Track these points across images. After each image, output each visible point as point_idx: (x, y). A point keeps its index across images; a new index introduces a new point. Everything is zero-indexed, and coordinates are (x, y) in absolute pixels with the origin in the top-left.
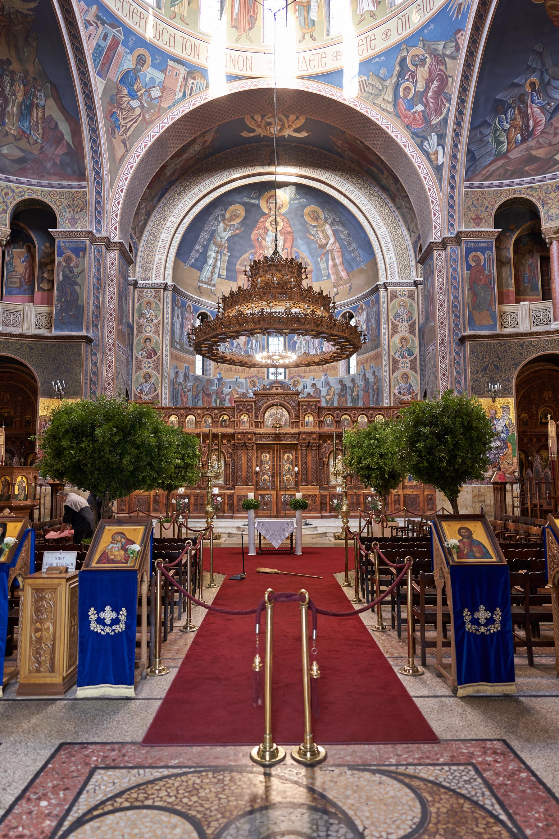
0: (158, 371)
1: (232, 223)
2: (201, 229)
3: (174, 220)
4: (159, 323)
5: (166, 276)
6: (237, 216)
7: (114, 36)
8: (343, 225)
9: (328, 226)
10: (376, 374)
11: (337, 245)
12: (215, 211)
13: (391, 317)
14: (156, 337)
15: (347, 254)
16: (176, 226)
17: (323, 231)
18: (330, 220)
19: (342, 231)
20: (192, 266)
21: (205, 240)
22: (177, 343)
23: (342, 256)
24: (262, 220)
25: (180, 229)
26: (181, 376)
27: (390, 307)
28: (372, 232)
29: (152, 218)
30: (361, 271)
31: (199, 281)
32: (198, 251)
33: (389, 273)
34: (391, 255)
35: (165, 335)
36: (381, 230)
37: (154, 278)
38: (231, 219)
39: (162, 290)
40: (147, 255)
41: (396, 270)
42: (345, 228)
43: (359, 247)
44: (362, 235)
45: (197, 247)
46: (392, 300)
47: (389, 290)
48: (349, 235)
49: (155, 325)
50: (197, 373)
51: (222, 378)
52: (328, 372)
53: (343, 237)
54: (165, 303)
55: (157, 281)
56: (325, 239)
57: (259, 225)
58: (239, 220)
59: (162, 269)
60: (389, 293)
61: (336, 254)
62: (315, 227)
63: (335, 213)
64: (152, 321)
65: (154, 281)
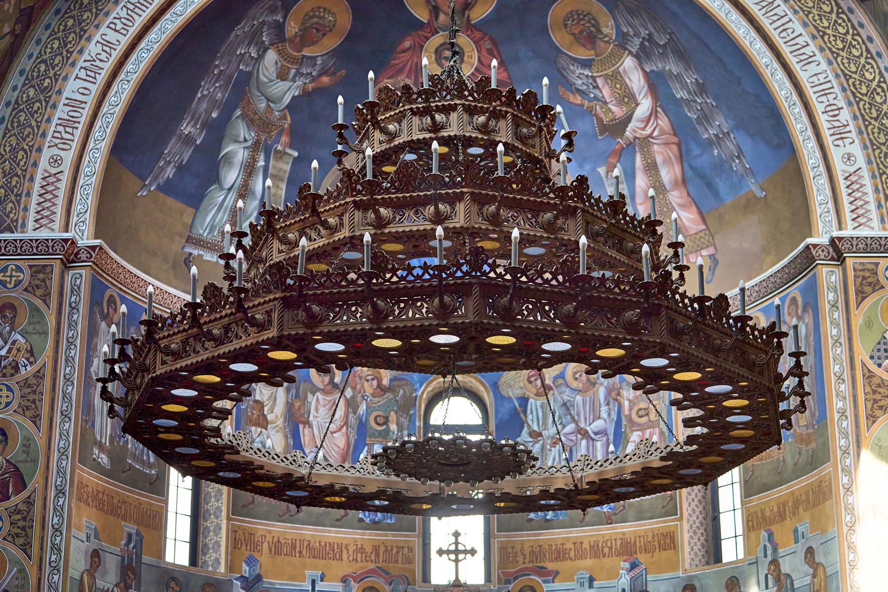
0: (25, 548)
1: (306, 52)
2: (202, 69)
3: (112, 36)
4: (39, 375)
5: (74, 219)
6: (324, 30)
7: (745, 498)
8: (682, 56)
9: (629, 63)
10: (819, 558)
11: (664, 122)
12: (252, 12)
13: (862, 354)
14: (29, 425)
15: (696, 151)
16: (116, 55)
17: (616, 78)
18: (637, 41)
19: (678, 78)
20: (168, 188)
21: (214, 104)
22: (101, 447)
23: (681, 158)
24: (407, 44)
25: (129, 66)
26: (111, 564)
27: (858, 321)
28: (781, 75)
29: (39, 32)
30: (750, 204)
31: (190, 240)
32: (188, 140)
33: (847, 208)
34: (850, 149)
35: (58, 418)
36: (812, 68)
37: (31, 224)
38: (305, 38)
39: (57, 267)
40: (14, 150)
41: (871, 197)
42: (688, 67)
43: (739, 126)
44: (748, 86)
45: (186, 128)
46: (862, 296)
47: (849, 262)
48: (702, 89)
49: (26, 383)
50: (169, 558)
51: (259, 578)
52: (642, 558)
53: (680, 94)
54: (66, 309)
55: (44, 234)
56: (620, 102)
57: (401, 59)
58: (331, 43)
59: (62, 194)
60: (851, 274)
61: (659, 153)
62: (586, 64)
63: (654, 19)
64: (16, 368)
65: (30, 234)
